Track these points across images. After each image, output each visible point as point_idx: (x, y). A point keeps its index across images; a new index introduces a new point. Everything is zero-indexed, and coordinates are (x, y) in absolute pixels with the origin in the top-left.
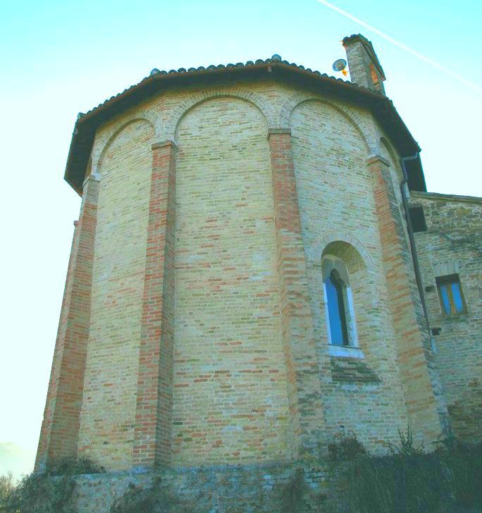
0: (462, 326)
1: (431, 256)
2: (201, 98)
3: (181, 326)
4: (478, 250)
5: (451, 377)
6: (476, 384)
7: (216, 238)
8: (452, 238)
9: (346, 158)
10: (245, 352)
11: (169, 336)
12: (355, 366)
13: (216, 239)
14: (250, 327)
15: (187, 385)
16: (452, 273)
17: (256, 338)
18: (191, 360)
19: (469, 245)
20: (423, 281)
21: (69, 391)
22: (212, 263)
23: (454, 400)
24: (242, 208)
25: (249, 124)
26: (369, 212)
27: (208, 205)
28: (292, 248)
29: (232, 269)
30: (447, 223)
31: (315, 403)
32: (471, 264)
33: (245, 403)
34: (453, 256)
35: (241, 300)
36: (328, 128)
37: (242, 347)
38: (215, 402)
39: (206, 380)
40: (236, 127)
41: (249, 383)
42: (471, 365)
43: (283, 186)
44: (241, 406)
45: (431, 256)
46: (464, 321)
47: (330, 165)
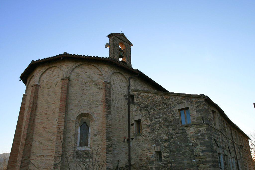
0: (139, 137)
1: (134, 113)
2: (47, 68)
3: (34, 141)
4: (148, 110)
5: (134, 155)
6: (141, 157)
7: (46, 114)
8: (141, 106)
9: (94, 83)
10: (49, 149)
11: (29, 145)
12: (85, 153)
13: (46, 115)
14: (51, 142)
15: (33, 159)
16: (139, 119)
17: (52, 145)
18: (35, 152)
19: (146, 109)
20: (131, 121)
21: (13, 161)
22: (44, 122)
23: (134, 162)
24: (54, 104)
25: (59, 76)
26: (100, 102)
27: (45, 104)
28: (61, 118)
29: (48, 124)
30: (141, 101)
31: (59, 165)
32: (145, 116)
33: (47, 165)
34: (140, 113)
35: (50, 134)
36: (88, 73)
37: (48, 148)
38: (39, 164)
39: (38, 158)
40: (56, 77)
41: (49, 159)
42: (140, 151)
43: (62, 97)
44: (46, 166)
45: (134, 113)
46: (140, 136)
47: (86, 87)
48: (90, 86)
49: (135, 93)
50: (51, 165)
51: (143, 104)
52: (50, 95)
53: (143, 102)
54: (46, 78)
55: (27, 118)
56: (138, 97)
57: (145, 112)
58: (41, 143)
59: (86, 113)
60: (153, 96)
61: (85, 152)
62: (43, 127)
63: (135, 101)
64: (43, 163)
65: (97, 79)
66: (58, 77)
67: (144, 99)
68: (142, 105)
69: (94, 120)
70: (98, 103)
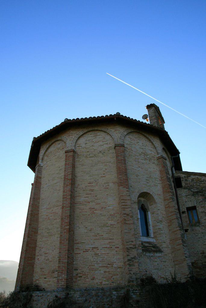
1: (184, 198)
2: (86, 131)
6: (203, 253)
8: (193, 191)
9: (148, 157)
10: (105, 239)
11: (72, 232)
12: (152, 245)
13: (93, 191)
16: (193, 206)
17: (109, 233)
18: (82, 243)
20: (181, 209)
22: (91, 201)
23: (194, 260)
24: (104, 178)
27: (89, 177)
28: (125, 195)
30: (191, 184)
31: (135, 261)
33: (105, 261)
37: (103, 237)
38: (92, 261)
39: (88, 251)
44: (103, 262)
45: (184, 198)
46: (198, 226)
47: (141, 159)
48: (146, 159)
49: (182, 175)
50: (113, 261)
51: (195, 189)
52: (95, 165)
53: (194, 186)
54: (86, 144)
55: (65, 194)
56: (186, 180)
57: (201, 197)
58: (90, 231)
59: (146, 192)
60: (153, 186)
61: (152, 244)
62: (90, 208)
63: (183, 184)
64: (97, 258)
65: (150, 152)
66: (105, 143)
67: (195, 183)
68: (194, 190)
69: (156, 203)
70: (156, 182)
